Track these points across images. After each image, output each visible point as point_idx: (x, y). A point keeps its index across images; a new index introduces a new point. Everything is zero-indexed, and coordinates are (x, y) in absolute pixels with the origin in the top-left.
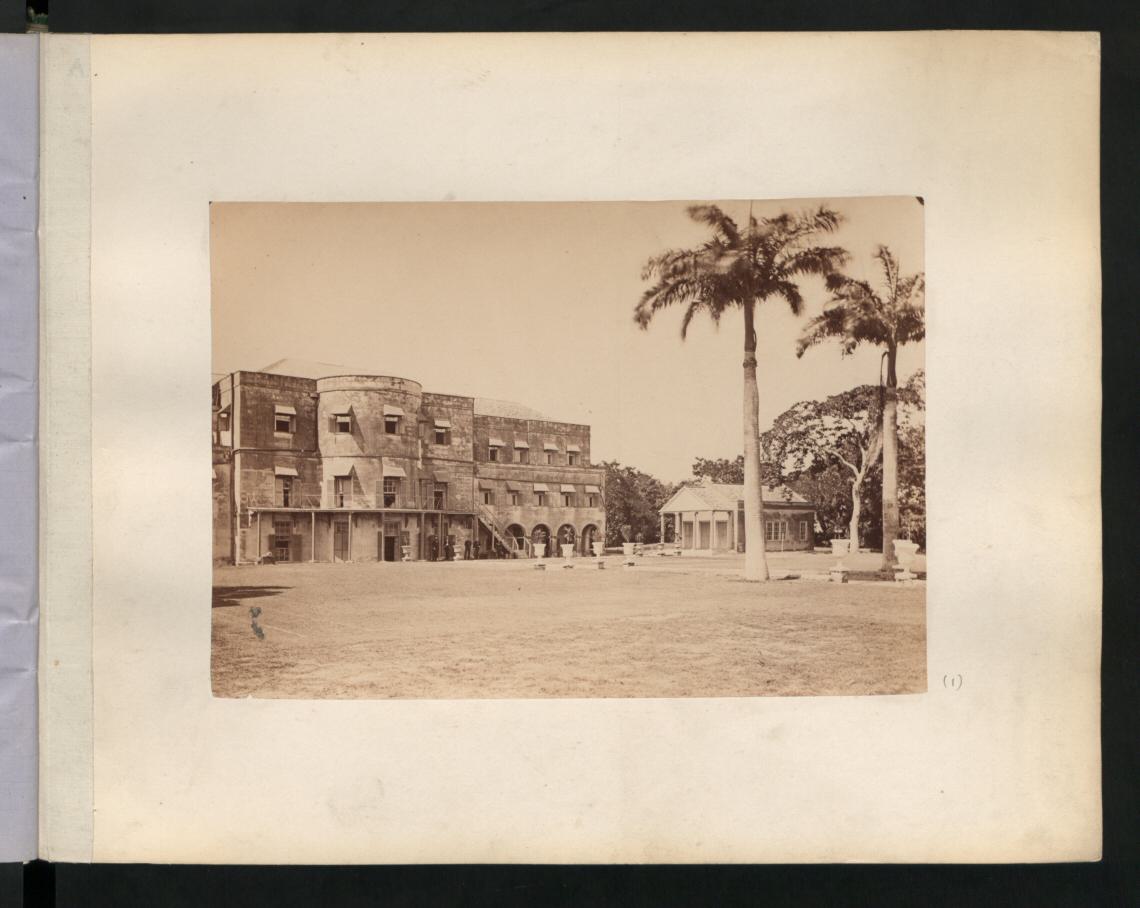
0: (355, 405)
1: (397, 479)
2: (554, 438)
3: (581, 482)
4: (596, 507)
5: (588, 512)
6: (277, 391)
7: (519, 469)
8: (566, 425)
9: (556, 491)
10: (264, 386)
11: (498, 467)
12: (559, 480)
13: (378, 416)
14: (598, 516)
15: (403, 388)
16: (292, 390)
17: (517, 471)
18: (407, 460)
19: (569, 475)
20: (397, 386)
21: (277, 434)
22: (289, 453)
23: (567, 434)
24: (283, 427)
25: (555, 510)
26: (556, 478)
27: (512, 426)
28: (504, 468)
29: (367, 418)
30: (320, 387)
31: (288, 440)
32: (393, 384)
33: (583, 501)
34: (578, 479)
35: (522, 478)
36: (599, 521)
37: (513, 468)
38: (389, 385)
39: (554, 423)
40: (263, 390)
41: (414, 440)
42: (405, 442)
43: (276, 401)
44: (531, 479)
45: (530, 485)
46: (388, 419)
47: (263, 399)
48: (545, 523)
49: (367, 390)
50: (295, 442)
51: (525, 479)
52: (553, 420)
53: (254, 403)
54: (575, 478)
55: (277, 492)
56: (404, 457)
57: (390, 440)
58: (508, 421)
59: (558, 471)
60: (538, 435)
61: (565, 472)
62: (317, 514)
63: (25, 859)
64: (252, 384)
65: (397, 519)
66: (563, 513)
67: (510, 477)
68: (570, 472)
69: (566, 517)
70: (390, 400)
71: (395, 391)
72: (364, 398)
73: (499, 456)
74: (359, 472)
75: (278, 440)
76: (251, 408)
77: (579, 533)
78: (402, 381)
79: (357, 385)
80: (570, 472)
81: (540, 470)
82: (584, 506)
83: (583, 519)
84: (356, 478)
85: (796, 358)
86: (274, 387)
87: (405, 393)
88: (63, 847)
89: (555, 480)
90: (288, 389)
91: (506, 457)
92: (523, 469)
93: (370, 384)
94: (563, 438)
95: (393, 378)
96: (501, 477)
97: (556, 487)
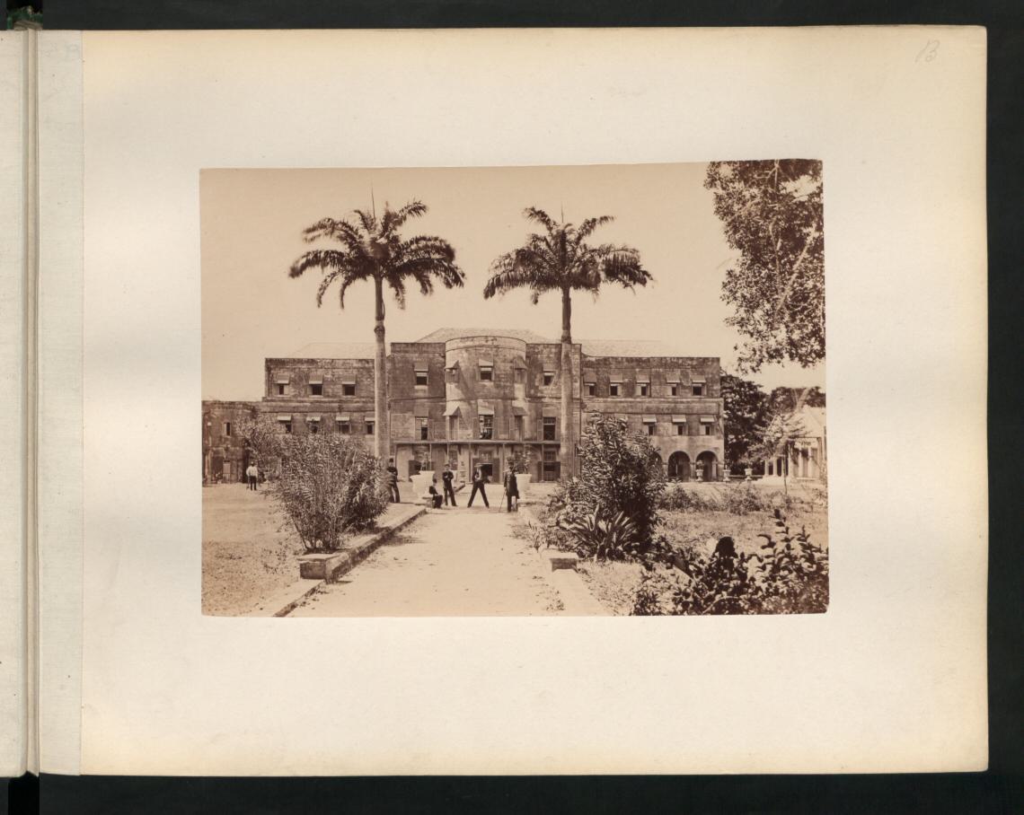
0: (460, 360)
1: (491, 416)
2: (678, 372)
3: (695, 412)
4: (712, 435)
5: (703, 441)
6: (417, 355)
7: (626, 402)
8: (692, 359)
9: (668, 421)
10: (407, 352)
11: (605, 402)
12: (670, 411)
13: (475, 368)
14: (716, 444)
15: (495, 343)
16: (427, 352)
17: (625, 405)
18: (500, 400)
19: (682, 406)
20: (490, 343)
21: (417, 387)
22: (426, 400)
23: (693, 367)
24: (421, 381)
25: (666, 439)
26: (668, 409)
27: (634, 364)
28: (612, 402)
29: (467, 369)
30: (448, 347)
31: (425, 391)
32: (487, 341)
33: (698, 430)
34: (692, 409)
35: (630, 410)
36: (716, 449)
37: (621, 402)
38: (484, 343)
39: (678, 358)
40: (407, 355)
41: (508, 384)
42: (498, 387)
43: (416, 362)
44: (638, 411)
45: (640, 416)
46: (483, 369)
47: (406, 361)
48: (684, 451)
49: (467, 348)
50: (430, 392)
51: (634, 411)
52: (678, 356)
53: (400, 365)
54: (688, 408)
55: (416, 430)
56: (497, 398)
57: (485, 386)
58: (630, 360)
59: (669, 402)
60: (661, 370)
61: (677, 402)
62: (433, 445)
63: (19, 773)
64: (399, 352)
65: (489, 449)
66: (675, 442)
67: (617, 410)
68: (682, 402)
69: (678, 444)
70: (484, 354)
71: (489, 346)
72: (465, 355)
73: (620, 391)
74: (463, 412)
75: (417, 391)
76: (398, 369)
77: (666, 459)
78: (495, 338)
79: (462, 345)
80: (682, 402)
81: (650, 402)
82: (698, 434)
83: (697, 447)
84: (461, 417)
85: (288, 271)
86: (415, 352)
87: (497, 347)
88: (61, 760)
89: (666, 411)
90: (425, 352)
91: (628, 391)
92: (631, 402)
93: (469, 343)
94: (689, 371)
95: (486, 337)
96: (609, 410)
97: (666, 417)
